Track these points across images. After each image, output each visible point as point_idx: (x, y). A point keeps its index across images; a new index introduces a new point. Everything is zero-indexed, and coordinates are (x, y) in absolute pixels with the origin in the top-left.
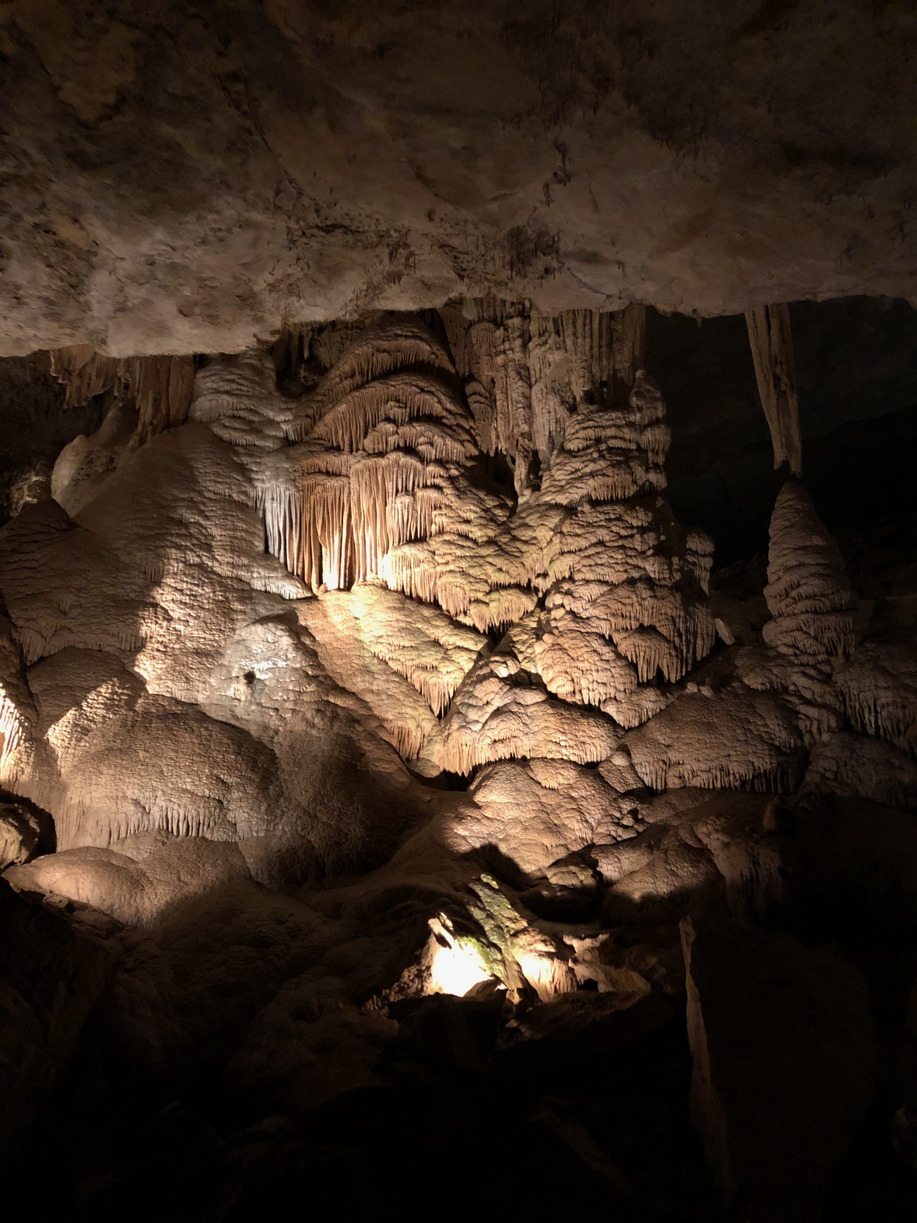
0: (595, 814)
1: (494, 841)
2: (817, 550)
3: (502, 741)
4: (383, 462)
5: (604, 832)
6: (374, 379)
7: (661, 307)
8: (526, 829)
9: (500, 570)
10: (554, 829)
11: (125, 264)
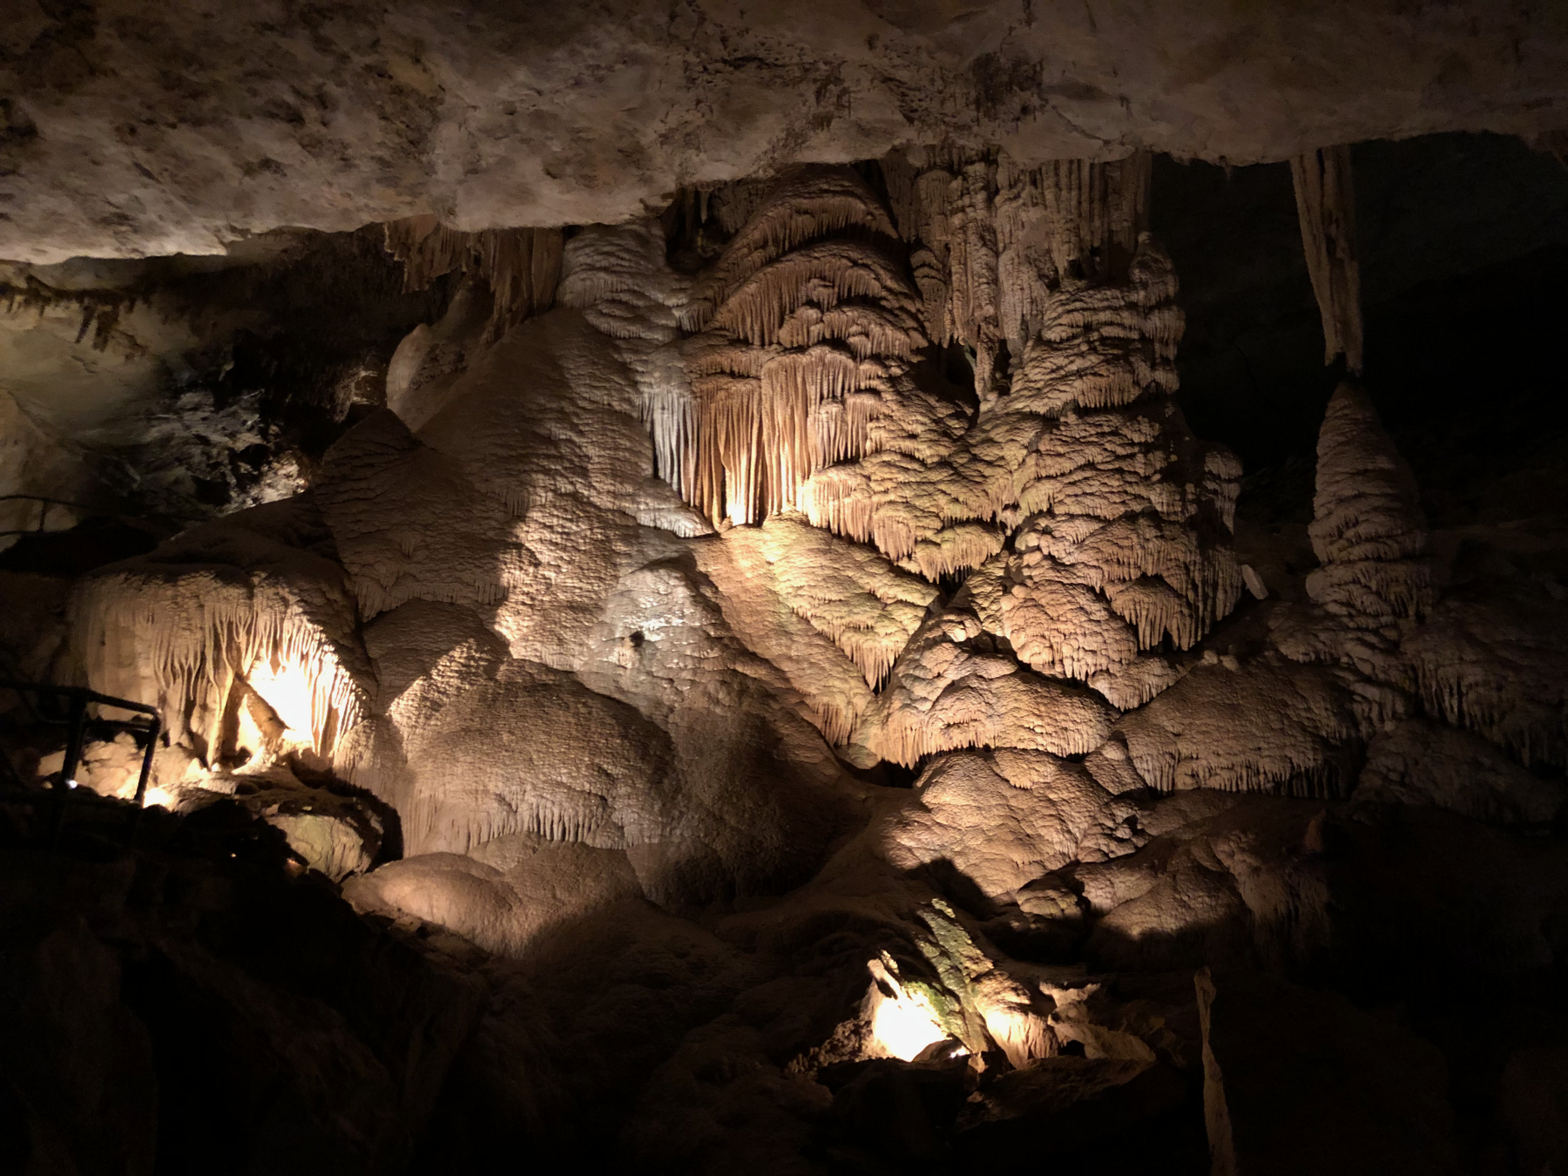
0: (1079, 823)
1: (948, 855)
2: (1382, 475)
3: (958, 725)
4: (804, 359)
5: (1092, 847)
6: (792, 249)
7: (1176, 154)
8: (989, 840)
9: (956, 500)
10: (1027, 841)
11: (478, 114)
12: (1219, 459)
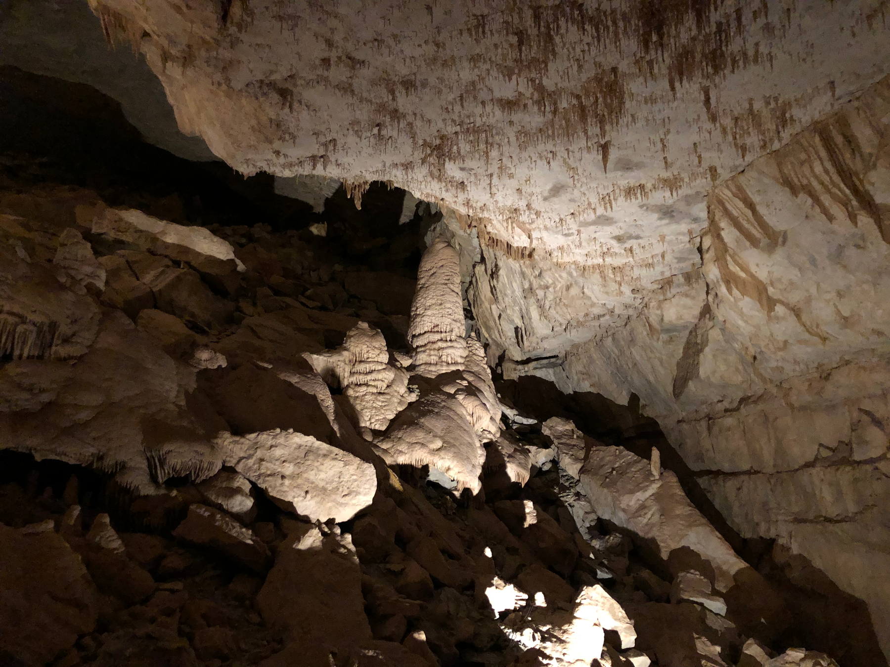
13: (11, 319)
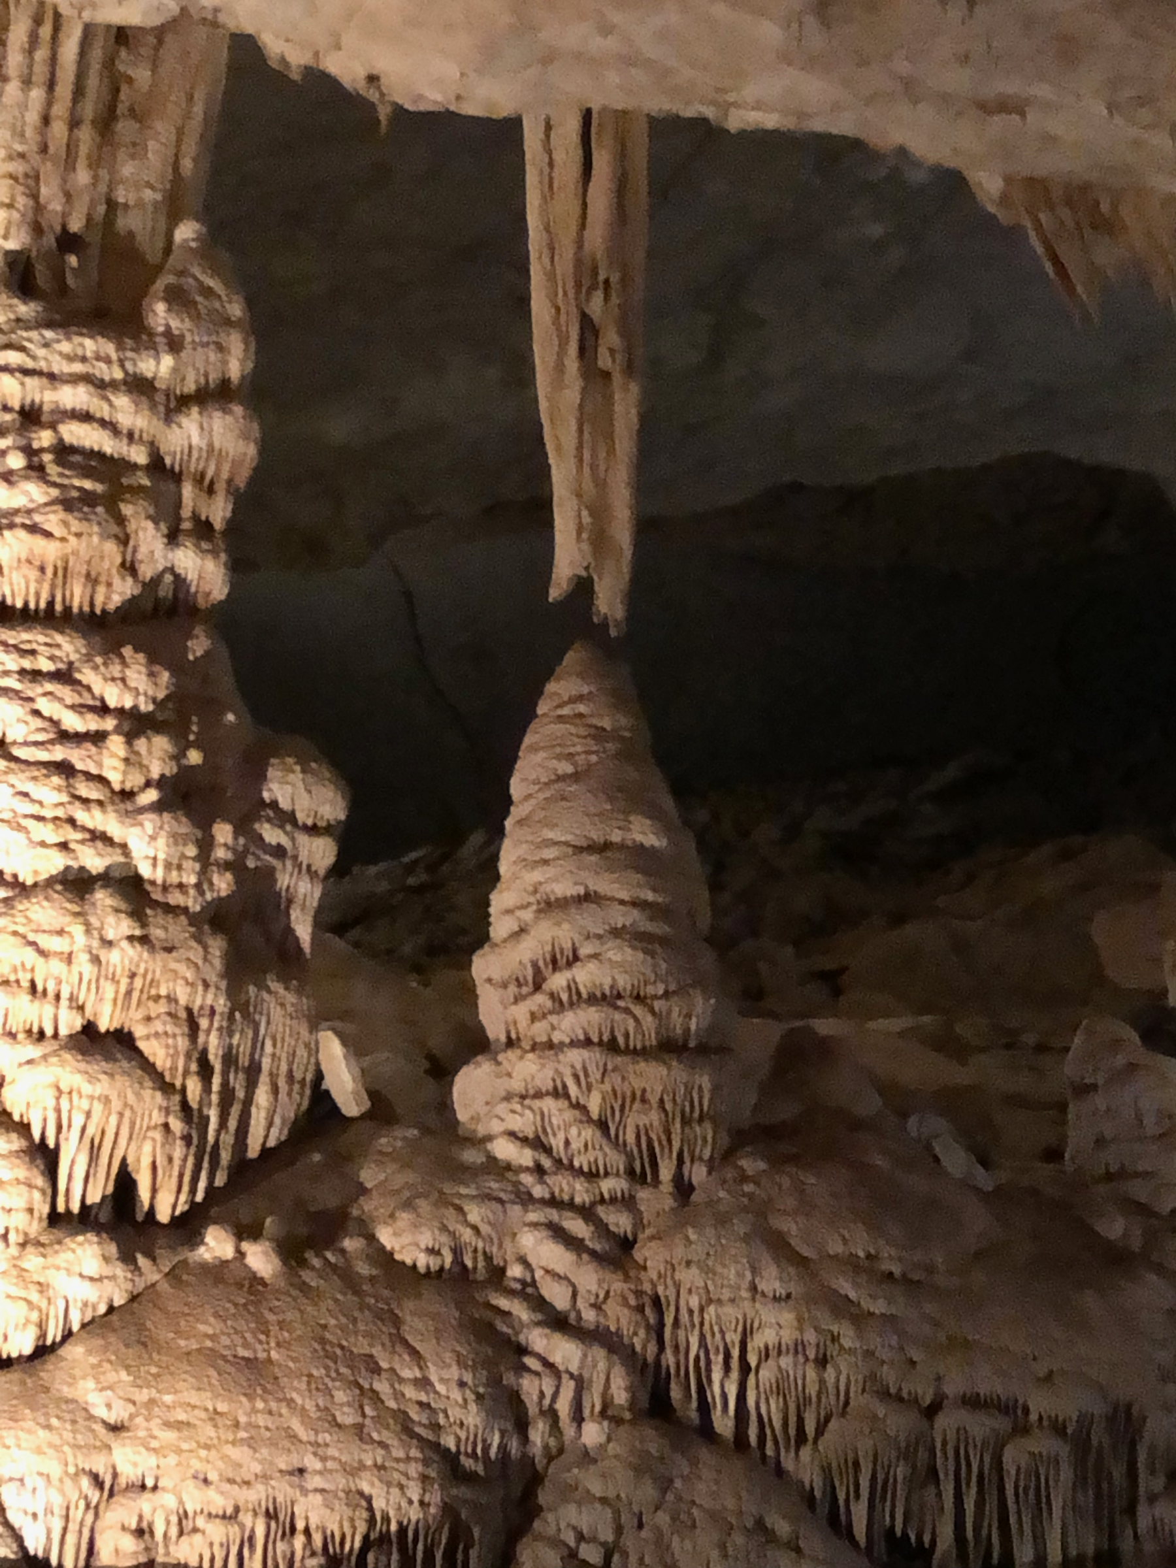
2: (639, 859)
12: (297, 777)
13: (980, 1426)
